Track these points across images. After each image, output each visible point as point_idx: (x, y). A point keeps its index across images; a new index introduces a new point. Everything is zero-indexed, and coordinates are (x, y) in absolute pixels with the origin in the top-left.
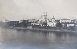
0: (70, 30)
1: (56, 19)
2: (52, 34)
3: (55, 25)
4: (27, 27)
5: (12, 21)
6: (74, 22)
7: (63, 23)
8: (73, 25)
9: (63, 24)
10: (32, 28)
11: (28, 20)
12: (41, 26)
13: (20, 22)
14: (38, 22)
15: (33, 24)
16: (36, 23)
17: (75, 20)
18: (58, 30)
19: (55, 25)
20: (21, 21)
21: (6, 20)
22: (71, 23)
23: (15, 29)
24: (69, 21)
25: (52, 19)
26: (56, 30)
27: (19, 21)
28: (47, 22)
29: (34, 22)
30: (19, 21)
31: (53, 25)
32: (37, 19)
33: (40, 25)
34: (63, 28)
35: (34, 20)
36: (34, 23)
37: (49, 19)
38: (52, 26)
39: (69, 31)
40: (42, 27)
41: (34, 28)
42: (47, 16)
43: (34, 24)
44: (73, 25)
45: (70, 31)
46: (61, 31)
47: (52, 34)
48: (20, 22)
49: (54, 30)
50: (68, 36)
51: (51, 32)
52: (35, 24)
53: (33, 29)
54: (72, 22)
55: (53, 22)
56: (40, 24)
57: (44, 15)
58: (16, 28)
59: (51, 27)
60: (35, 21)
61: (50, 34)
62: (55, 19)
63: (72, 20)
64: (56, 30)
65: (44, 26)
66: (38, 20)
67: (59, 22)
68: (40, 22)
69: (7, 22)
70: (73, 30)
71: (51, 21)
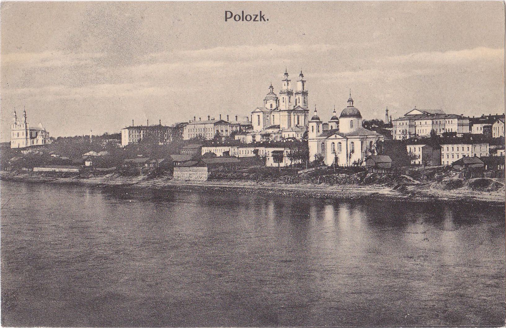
0: (457, 185)
1: (367, 117)
2: (344, 212)
3: (357, 156)
4: (177, 173)
5: (476, 125)
6: (488, 130)
7: (415, 140)
8: (483, 150)
9: (417, 150)
10: (210, 178)
11: (179, 128)
12: (271, 162)
13: (125, 141)
14: (249, 139)
15: (212, 149)
16: (231, 142)
17: (497, 118)
18: (386, 191)
19: (357, 156)
20: (137, 136)
21: (32, 134)
22: (467, 139)
23: (93, 188)
24: (453, 126)
25: (343, 115)
26: (368, 190)
27: (118, 136)
28: (306, 135)
29: (218, 136)
30: (118, 136)
31: (349, 156)
32: (242, 121)
33: (265, 159)
34: (416, 175)
35: (221, 122)
36: (216, 141)
37: (325, 119)
38: (343, 162)
39: (454, 193)
40: (274, 174)
41: (219, 178)
42: (305, 94)
43: (219, 151)
44: (483, 150)
45: (464, 192)
46: (403, 190)
47: (344, 212)
48: (125, 141)
49: (354, 190)
50: (448, 223)
51: (337, 203)
52: (233, 151)
53: (215, 184)
54: (477, 129)
55: (345, 137)
56: (262, 151)
57: (290, 93)
58: (98, 180)
59: (336, 168)
60: (226, 131)
61: (329, 211)
62: (358, 115)
63: (474, 121)
64: (368, 190)
65: (287, 162)
66: (250, 127)
67: (388, 134)
68: (258, 139)
69: (39, 141)
70: (482, 185)
71: (335, 132)
